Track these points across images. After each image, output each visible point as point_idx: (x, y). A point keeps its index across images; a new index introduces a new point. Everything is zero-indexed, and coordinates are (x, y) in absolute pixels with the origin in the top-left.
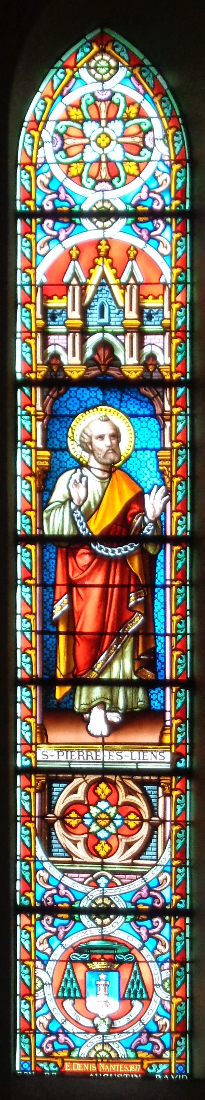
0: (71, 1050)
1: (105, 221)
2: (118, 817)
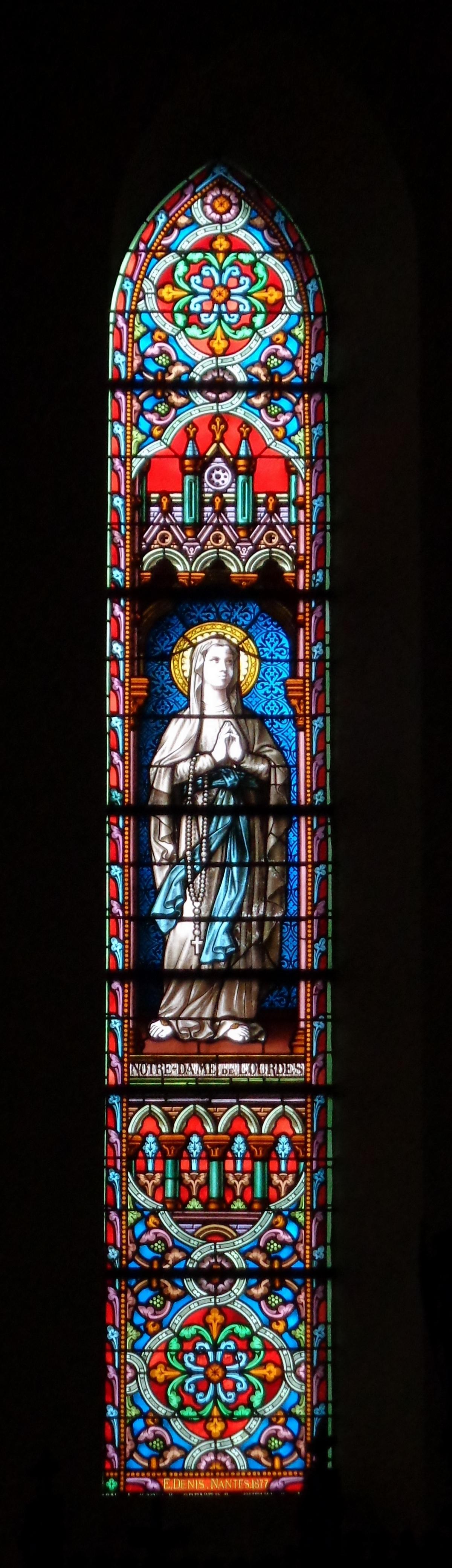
1: (221, 393)
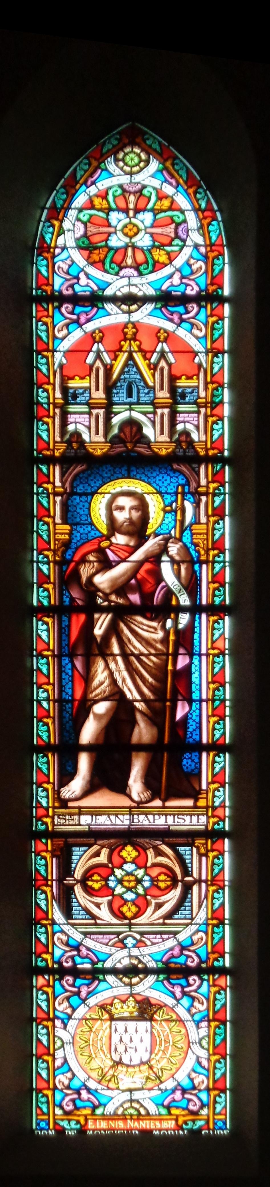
0: (94, 1108)
1: (132, 305)
2: (147, 878)
